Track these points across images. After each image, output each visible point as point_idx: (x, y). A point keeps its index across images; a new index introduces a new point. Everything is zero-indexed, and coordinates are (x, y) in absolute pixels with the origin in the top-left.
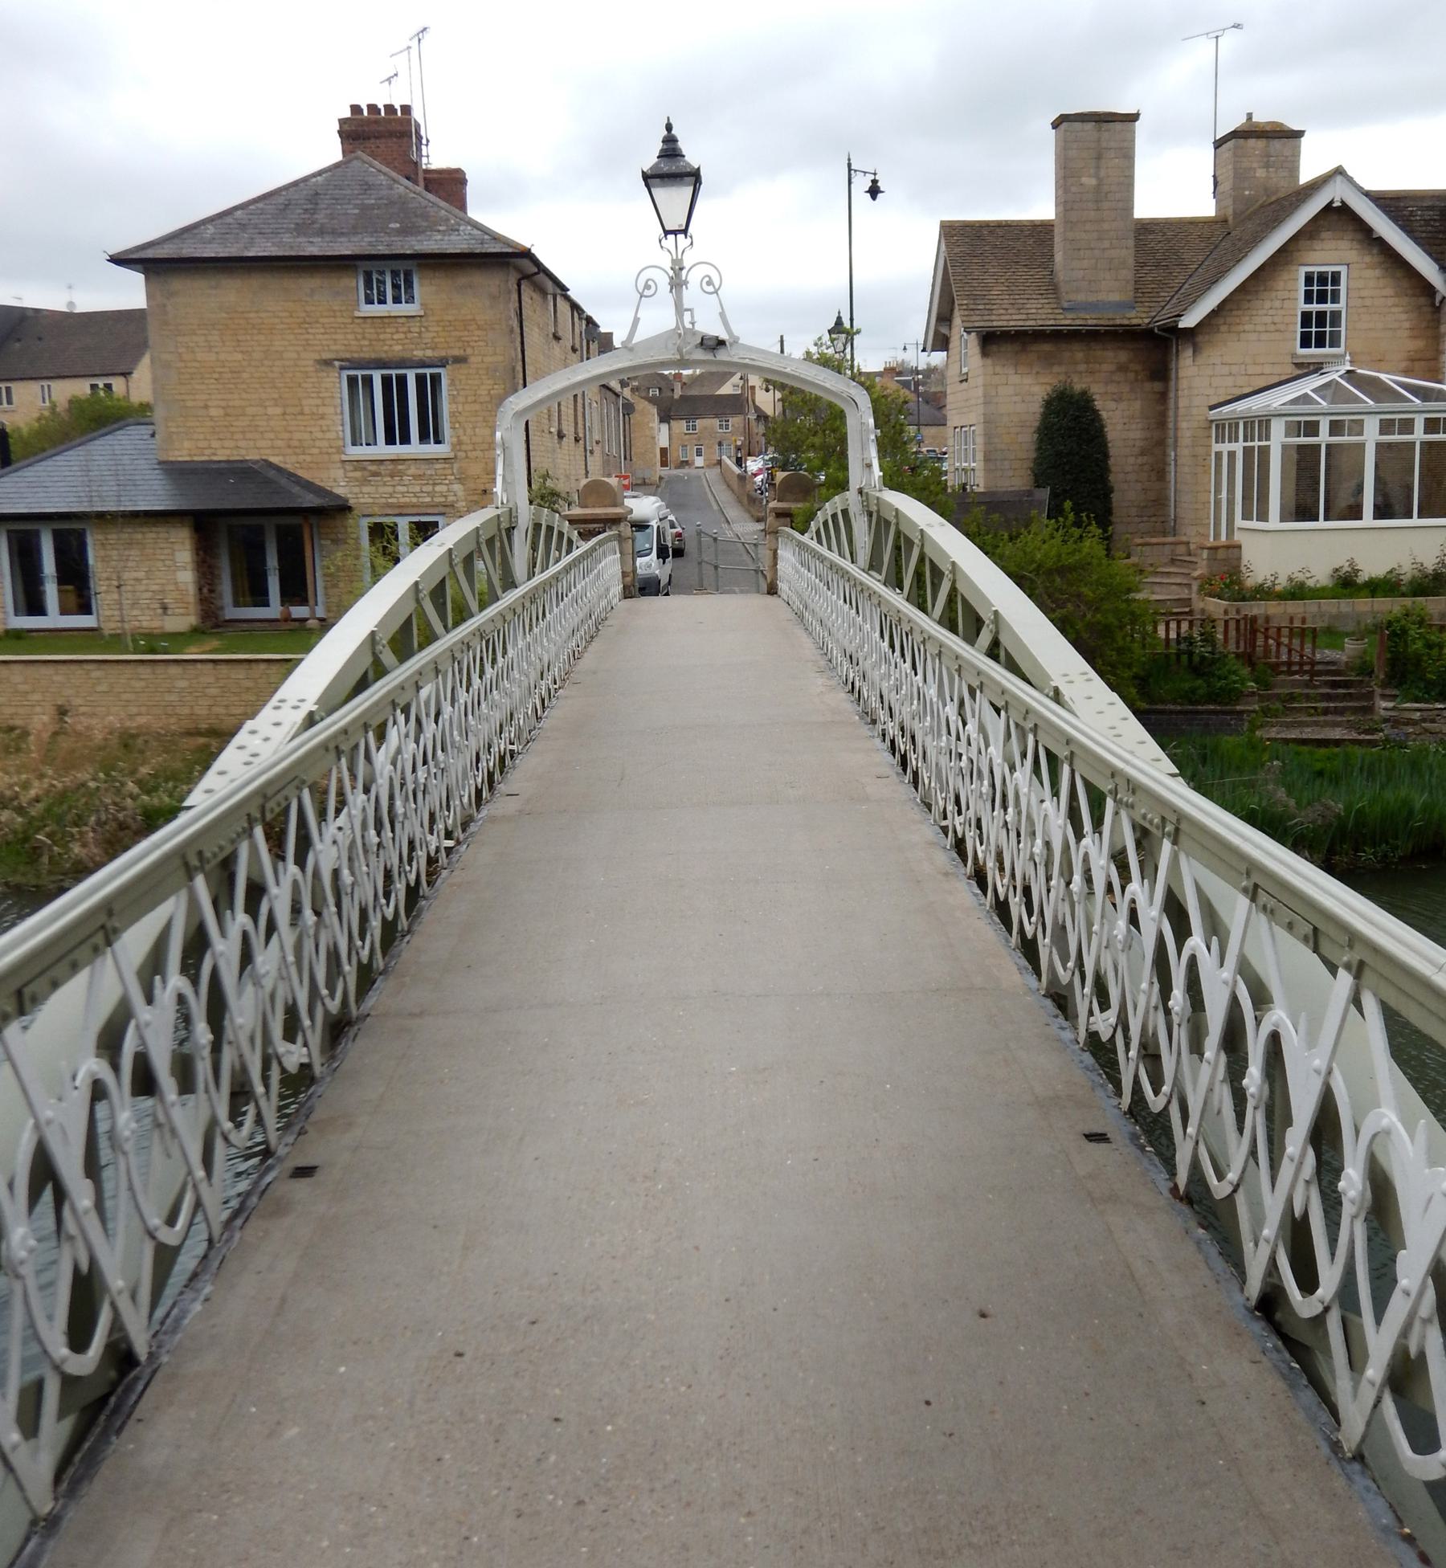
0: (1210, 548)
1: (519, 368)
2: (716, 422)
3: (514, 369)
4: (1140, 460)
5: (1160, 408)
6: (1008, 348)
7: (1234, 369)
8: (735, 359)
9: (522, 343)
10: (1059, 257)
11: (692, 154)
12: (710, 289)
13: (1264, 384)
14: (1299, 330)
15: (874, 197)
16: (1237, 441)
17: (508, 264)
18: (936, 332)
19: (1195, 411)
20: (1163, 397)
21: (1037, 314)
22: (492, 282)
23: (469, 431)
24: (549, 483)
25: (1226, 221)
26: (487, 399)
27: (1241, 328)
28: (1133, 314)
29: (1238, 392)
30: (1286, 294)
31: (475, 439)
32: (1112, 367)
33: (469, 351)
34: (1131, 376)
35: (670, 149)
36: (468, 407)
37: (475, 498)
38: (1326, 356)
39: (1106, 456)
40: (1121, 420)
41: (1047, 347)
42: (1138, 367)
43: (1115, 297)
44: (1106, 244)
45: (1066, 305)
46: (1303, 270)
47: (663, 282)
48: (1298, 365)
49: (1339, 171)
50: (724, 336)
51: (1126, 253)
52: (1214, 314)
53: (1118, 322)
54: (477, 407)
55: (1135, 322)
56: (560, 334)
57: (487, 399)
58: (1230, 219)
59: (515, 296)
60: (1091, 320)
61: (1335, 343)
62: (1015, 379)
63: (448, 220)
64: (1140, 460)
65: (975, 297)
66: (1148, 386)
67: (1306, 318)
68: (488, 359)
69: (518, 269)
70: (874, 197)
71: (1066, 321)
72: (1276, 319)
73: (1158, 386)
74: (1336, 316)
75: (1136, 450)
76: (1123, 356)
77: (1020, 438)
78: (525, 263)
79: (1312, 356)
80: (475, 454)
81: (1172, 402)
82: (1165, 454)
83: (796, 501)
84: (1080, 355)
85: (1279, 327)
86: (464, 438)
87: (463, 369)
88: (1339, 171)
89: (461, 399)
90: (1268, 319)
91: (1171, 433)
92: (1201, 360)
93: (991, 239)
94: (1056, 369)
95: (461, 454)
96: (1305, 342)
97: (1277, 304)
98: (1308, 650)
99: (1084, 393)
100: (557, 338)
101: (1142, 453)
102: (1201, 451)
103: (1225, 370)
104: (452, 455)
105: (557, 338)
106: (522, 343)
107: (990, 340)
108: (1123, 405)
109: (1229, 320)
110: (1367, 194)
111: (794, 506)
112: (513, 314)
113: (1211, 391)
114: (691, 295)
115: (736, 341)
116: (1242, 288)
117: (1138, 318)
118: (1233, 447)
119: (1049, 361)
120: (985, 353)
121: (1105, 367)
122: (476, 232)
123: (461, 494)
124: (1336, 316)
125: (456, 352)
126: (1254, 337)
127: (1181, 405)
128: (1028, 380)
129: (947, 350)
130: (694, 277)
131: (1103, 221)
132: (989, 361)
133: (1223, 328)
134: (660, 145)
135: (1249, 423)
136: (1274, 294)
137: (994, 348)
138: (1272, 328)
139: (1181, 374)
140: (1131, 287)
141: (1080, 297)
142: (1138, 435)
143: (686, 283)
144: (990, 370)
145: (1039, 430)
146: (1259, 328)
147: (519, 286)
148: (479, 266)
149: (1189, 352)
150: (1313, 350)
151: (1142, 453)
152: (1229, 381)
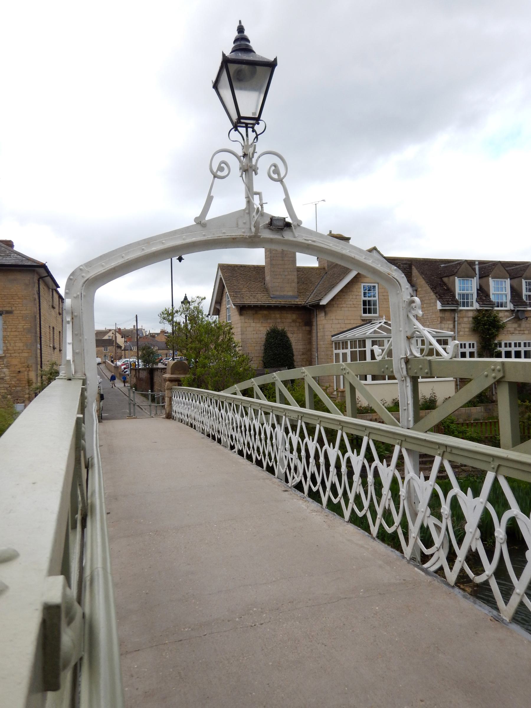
0: (341, 392)
1: (38, 316)
2: (103, 348)
3: (35, 316)
4: (302, 357)
5: (309, 336)
6: (250, 312)
7: (340, 321)
8: (300, 240)
9: (40, 306)
10: (268, 278)
11: (262, 50)
12: (275, 176)
13: (351, 327)
14: (362, 307)
15: (180, 261)
16: (347, 348)
17: (34, 271)
18: (215, 307)
19: (326, 337)
20: (310, 332)
21: (260, 299)
22: (27, 278)
23: (12, 344)
24: (55, 367)
25: (324, 269)
26: (22, 330)
27: (342, 306)
28: (297, 300)
29: (342, 330)
30: (357, 294)
31: (15, 348)
32: (290, 321)
33: (14, 308)
34: (298, 324)
35: (242, 43)
36: (12, 333)
37: (14, 375)
38: (373, 317)
39: (293, 355)
40: (296, 340)
41: (265, 312)
42: (300, 321)
43: (290, 294)
44: (286, 273)
45: (272, 296)
46: (363, 285)
47: (235, 164)
48: (363, 320)
49: (375, 249)
50: (289, 220)
51: (294, 277)
52: (332, 300)
53: (293, 303)
54: (17, 333)
55: (299, 303)
56: (55, 306)
57: (22, 330)
58: (326, 268)
59: (37, 285)
60: (282, 302)
61: (375, 312)
62: (253, 325)
63: (5, 251)
64: (302, 357)
65: (236, 292)
66: (304, 328)
67: (364, 302)
68: (23, 312)
69: (38, 273)
70: (180, 261)
71: (273, 302)
72: (355, 303)
73: (308, 328)
74: (375, 302)
75: (301, 353)
76: (294, 316)
77: (256, 348)
78: (42, 271)
79: (368, 317)
80: (15, 355)
81: (314, 335)
82: (311, 354)
83: (180, 374)
84: (278, 316)
85: (355, 306)
86: (10, 348)
87: (10, 316)
88: (375, 249)
89: (9, 330)
90: (351, 303)
91: (315, 346)
92: (327, 318)
93: (239, 271)
94: (269, 321)
95: (8, 355)
96: (365, 312)
97: (354, 297)
98: (24, 382)
99: (283, 330)
100: (53, 307)
101: (303, 354)
102: (330, 353)
103: (336, 321)
104: (3, 355)
105: (53, 307)
106: (40, 306)
107: (242, 309)
108: (295, 335)
109: (337, 303)
110: (385, 258)
111: (181, 376)
112: (36, 293)
113: (332, 330)
114: (260, 182)
115: (299, 224)
116: (342, 291)
117: (300, 301)
118: (345, 351)
119: (266, 317)
120: (241, 314)
121: (288, 320)
122: (19, 256)
123: (7, 373)
124: (375, 302)
125: (7, 309)
126: (346, 309)
127: (319, 335)
128: (258, 325)
129: (218, 315)
130: (263, 164)
131: (285, 264)
132: (243, 317)
133: (335, 306)
134: (233, 45)
135: (353, 343)
136: (353, 293)
137: (245, 312)
138: (353, 306)
139: (318, 323)
140: (296, 290)
141: (278, 293)
142: (301, 347)
143: (255, 170)
144: (243, 321)
145: (265, 345)
146: (348, 306)
147: (39, 281)
148: (20, 271)
149: (323, 314)
150: (367, 315)
151: (303, 354)
152: (338, 326)
